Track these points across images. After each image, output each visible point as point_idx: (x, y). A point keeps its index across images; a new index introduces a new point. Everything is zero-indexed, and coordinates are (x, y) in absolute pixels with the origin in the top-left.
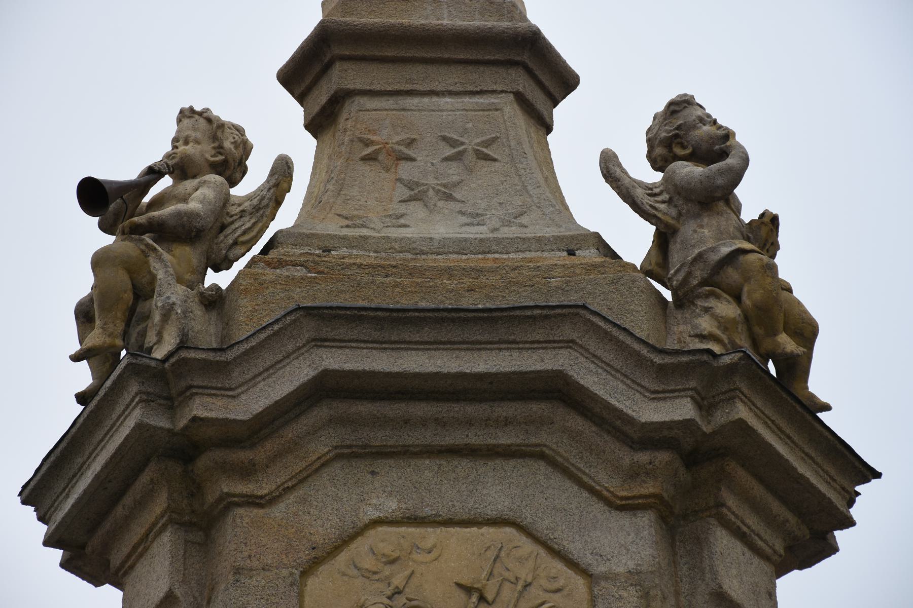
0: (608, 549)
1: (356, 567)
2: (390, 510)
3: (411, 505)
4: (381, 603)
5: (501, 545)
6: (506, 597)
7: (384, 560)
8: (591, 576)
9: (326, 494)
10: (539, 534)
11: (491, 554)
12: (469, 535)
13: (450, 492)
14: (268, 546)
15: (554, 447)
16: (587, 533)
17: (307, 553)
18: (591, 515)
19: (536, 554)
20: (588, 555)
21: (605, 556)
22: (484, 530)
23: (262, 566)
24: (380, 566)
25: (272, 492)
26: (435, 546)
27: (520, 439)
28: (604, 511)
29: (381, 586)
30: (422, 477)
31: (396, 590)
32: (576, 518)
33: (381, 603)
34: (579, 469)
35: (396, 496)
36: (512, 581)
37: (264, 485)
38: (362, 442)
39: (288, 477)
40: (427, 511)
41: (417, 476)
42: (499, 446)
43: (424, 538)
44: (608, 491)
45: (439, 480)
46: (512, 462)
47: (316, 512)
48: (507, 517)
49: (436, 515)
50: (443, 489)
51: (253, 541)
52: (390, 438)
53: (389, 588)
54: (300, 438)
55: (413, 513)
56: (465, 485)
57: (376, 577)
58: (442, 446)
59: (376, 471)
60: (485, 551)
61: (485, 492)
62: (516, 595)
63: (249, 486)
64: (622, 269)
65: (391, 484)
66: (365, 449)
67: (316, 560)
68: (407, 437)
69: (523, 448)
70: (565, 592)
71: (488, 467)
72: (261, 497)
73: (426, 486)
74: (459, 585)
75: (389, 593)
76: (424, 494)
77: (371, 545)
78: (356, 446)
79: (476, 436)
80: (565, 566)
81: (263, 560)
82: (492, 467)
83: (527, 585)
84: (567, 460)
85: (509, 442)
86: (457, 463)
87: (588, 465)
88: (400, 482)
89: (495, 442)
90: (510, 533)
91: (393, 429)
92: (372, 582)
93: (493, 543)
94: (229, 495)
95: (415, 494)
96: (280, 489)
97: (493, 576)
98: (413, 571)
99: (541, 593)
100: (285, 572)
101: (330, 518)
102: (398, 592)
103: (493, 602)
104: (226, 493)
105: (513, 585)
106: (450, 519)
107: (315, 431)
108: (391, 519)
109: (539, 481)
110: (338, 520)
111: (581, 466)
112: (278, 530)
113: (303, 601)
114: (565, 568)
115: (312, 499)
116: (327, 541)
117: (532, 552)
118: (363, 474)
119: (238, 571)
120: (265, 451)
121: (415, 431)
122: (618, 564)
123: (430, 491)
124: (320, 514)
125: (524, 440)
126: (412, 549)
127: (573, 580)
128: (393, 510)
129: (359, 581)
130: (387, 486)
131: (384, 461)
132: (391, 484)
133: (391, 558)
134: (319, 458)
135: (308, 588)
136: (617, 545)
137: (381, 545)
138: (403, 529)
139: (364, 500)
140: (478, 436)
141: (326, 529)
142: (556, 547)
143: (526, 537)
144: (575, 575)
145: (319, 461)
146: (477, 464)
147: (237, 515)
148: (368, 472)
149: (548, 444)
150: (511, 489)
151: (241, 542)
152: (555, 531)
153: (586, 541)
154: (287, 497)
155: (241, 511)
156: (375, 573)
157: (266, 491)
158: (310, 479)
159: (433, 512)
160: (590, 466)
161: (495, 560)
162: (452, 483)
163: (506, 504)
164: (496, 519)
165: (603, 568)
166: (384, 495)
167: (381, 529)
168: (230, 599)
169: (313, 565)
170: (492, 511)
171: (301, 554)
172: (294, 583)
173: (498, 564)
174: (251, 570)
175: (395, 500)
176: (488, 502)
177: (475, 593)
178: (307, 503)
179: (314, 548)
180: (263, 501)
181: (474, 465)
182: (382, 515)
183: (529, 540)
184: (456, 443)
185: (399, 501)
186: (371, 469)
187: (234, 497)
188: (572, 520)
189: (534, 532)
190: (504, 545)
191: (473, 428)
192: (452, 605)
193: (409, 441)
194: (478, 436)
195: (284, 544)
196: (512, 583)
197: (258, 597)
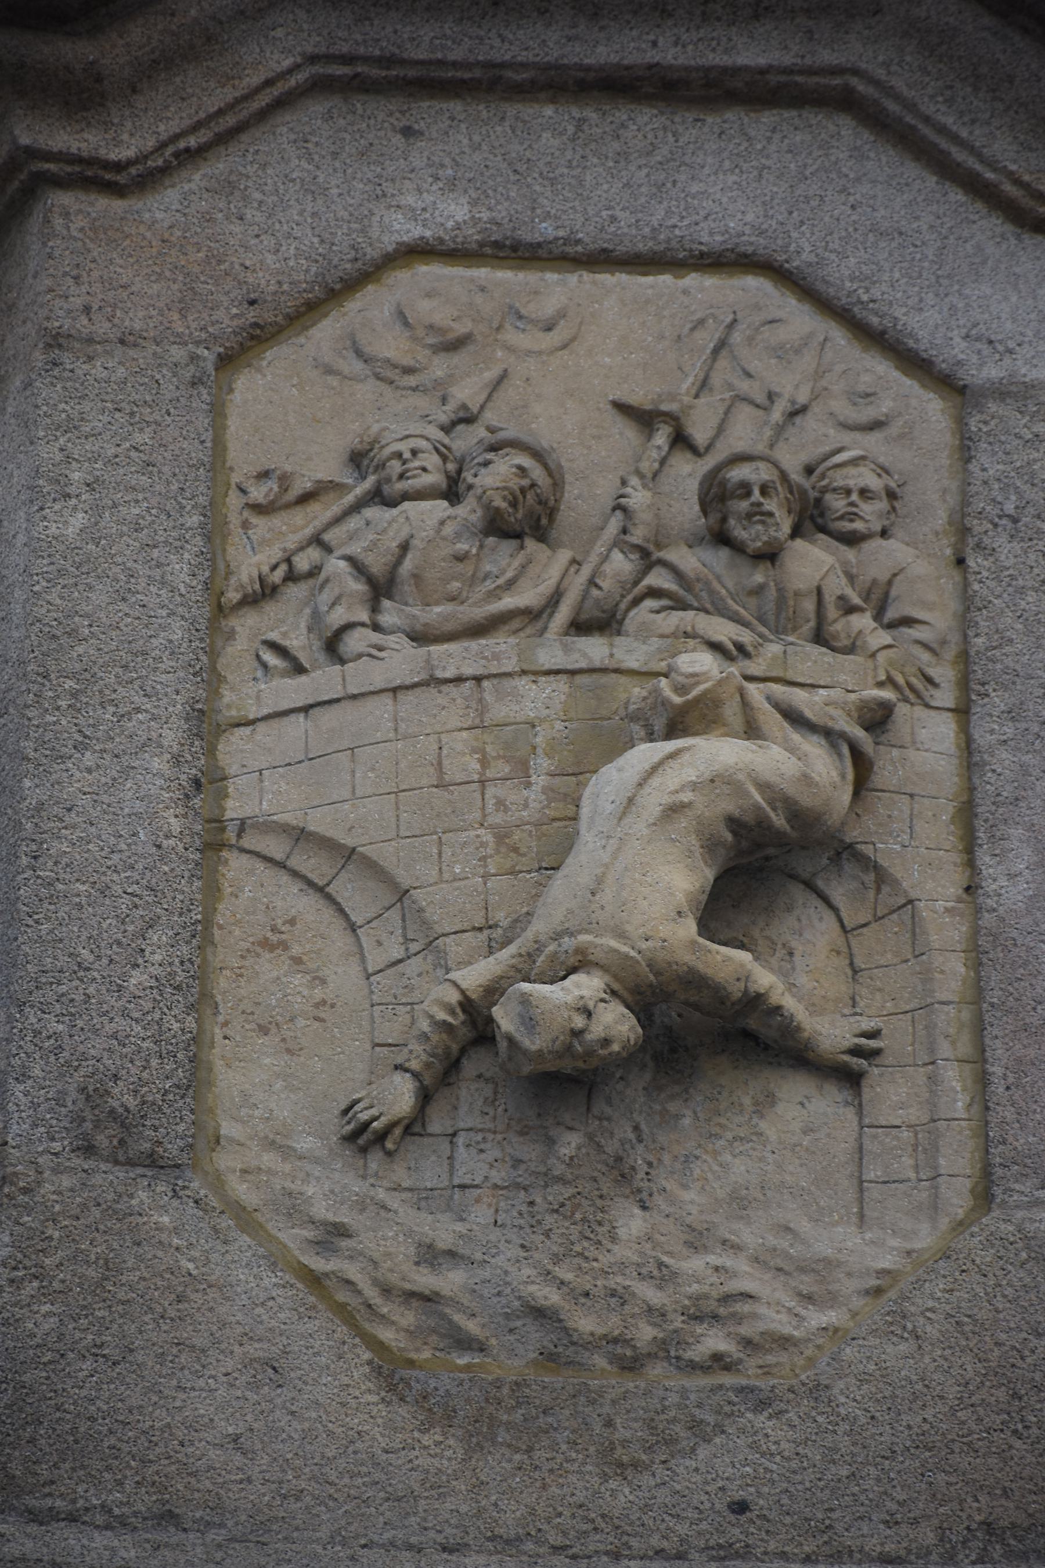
0: (1009, 325)
1: (359, 353)
2: (450, 224)
3: (504, 214)
4: (422, 436)
5: (731, 317)
6: (740, 438)
7: (431, 340)
8: (962, 391)
9: (286, 176)
10: (832, 291)
11: (707, 339)
12: (650, 291)
13: (605, 187)
14: (134, 289)
15: (880, 73)
16: (956, 287)
17: (234, 311)
18: (968, 246)
19: (822, 338)
20: (958, 340)
21: (1000, 342)
22: (692, 280)
23: (119, 335)
24: (422, 355)
25: (146, 157)
26: (562, 314)
27: (792, 53)
28: (1003, 236)
29: (422, 402)
30: (535, 146)
31: (461, 414)
32: (930, 253)
33: (422, 436)
34: (942, 130)
35: (466, 191)
36: (758, 401)
37: (125, 137)
38: (382, 49)
39: (187, 123)
40: (546, 230)
41: (522, 144)
42: (735, 71)
43: (536, 293)
44: (1017, 182)
45: (578, 157)
46: (768, 117)
47: (259, 217)
48: (750, 249)
49: (566, 241)
50: (588, 178)
51: (95, 274)
52: (454, 42)
53: (444, 408)
54: (221, 23)
55: (509, 234)
56: (645, 171)
57: (412, 380)
58: (588, 68)
59: (416, 127)
60: (693, 329)
61: (695, 188)
62: (768, 433)
63: (86, 136)
64: (542, 1421)
65: (454, 160)
66: (388, 68)
67: (258, 332)
68: (497, 43)
69: (799, 79)
70: (894, 430)
71: (706, 129)
72: (119, 167)
73: (545, 170)
74: (622, 408)
75: (444, 419)
76: (537, 188)
77: (399, 305)
78: (366, 60)
79: (676, 44)
80: (897, 368)
81: (123, 320)
82: (716, 129)
83: (797, 412)
84: (911, 107)
85: (762, 61)
86: (625, 117)
87: (966, 119)
88: (477, 157)
89: (725, 60)
90: (758, 289)
91: (462, 19)
92: (399, 393)
93: (712, 311)
94: (33, 153)
95: (515, 188)
96: (170, 150)
97: (711, 390)
98: (506, 371)
99: (832, 431)
100: (178, 353)
101: (297, 233)
102: (467, 418)
103: (709, 448)
104: (27, 147)
105: (761, 412)
106: (604, 250)
107: (260, 10)
108: (452, 246)
109: (836, 163)
110: (316, 240)
111: (949, 121)
112: (160, 253)
113: (224, 427)
114: (896, 374)
115: (250, 184)
116: (285, 287)
117: (811, 335)
118: (382, 133)
119: (56, 341)
120: (128, 44)
121: (519, 27)
122: (1035, 361)
123: (553, 182)
124: (270, 222)
125: (803, 57)
126: (503, 318)
127: (914, 402)
128: (457, 223)
129: (367, 390)
130: (442, 166)
131: (438, 105)
132: (454, 160)
133: (450, 336)
134: (269, 83)
135: (237, 397)
136: (1033, 316)
137: (425, 305)
138: (482, 273)
139: (384, 195)
140: (684, 46)
141: (285, 259)
142: (875, 320)
143: (799, 301)
144: (921, 391)
145: (268, 91)
146: (677, 119)
147: (55, 209)
148: (394, 130)
149: (864, 66)
150: (764, 182)
151: (65, 274)
152: (874, 283)
153: (952, 308)
154: (184, 174)
155: (64, 199)
156: (408, 371)
157: (130, 153)
158: (244, 137)
159: (561, 233)
160: (973, 122)
161: (716, 351)
162: (611, 164)
163: (750, 217)
164: (721, 255)
165: (993, 372)
166: (435, 187)
167: (429, 271)
168: (37, 406)
169: (249, 344)
170: (711, 234)
171: (220, 314)
172: (200, 379)
173: (723, 363)
174: (90, 341)
175: (464, 200)
176: (702, 213)
177: (662, 425)
178: (237, 193)
179: (252, 303)
180: (122, 179)
181: (668, 123)
182: (428, 234)
183: (806, 307)
184: (625, 62)
185: (474, 203)
186: (404, 122)
187: (48, 161)
188: (918, 256)
189: (820, 286)
190: (739, 317)
191: (670, 23)
192: (603, 453)
193: (503, 53)
194: (684, 46)
195: (176, 287)
196: (758, 406)
197: (108, 405)
